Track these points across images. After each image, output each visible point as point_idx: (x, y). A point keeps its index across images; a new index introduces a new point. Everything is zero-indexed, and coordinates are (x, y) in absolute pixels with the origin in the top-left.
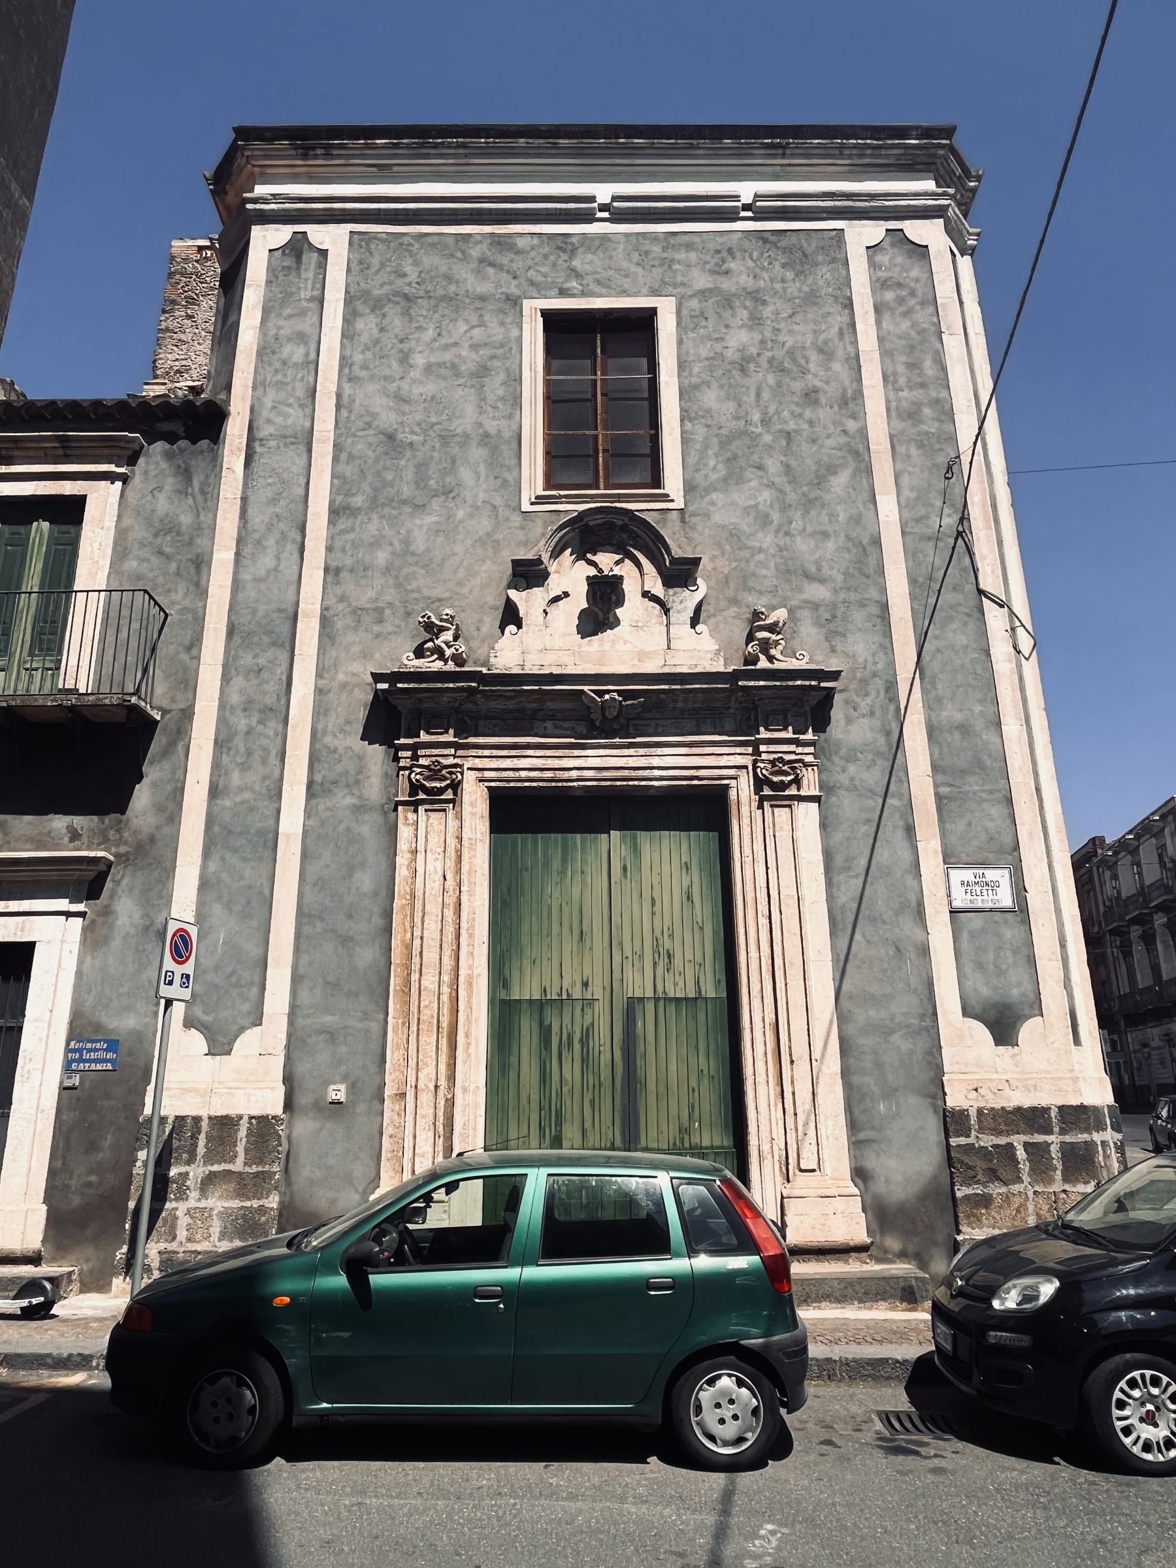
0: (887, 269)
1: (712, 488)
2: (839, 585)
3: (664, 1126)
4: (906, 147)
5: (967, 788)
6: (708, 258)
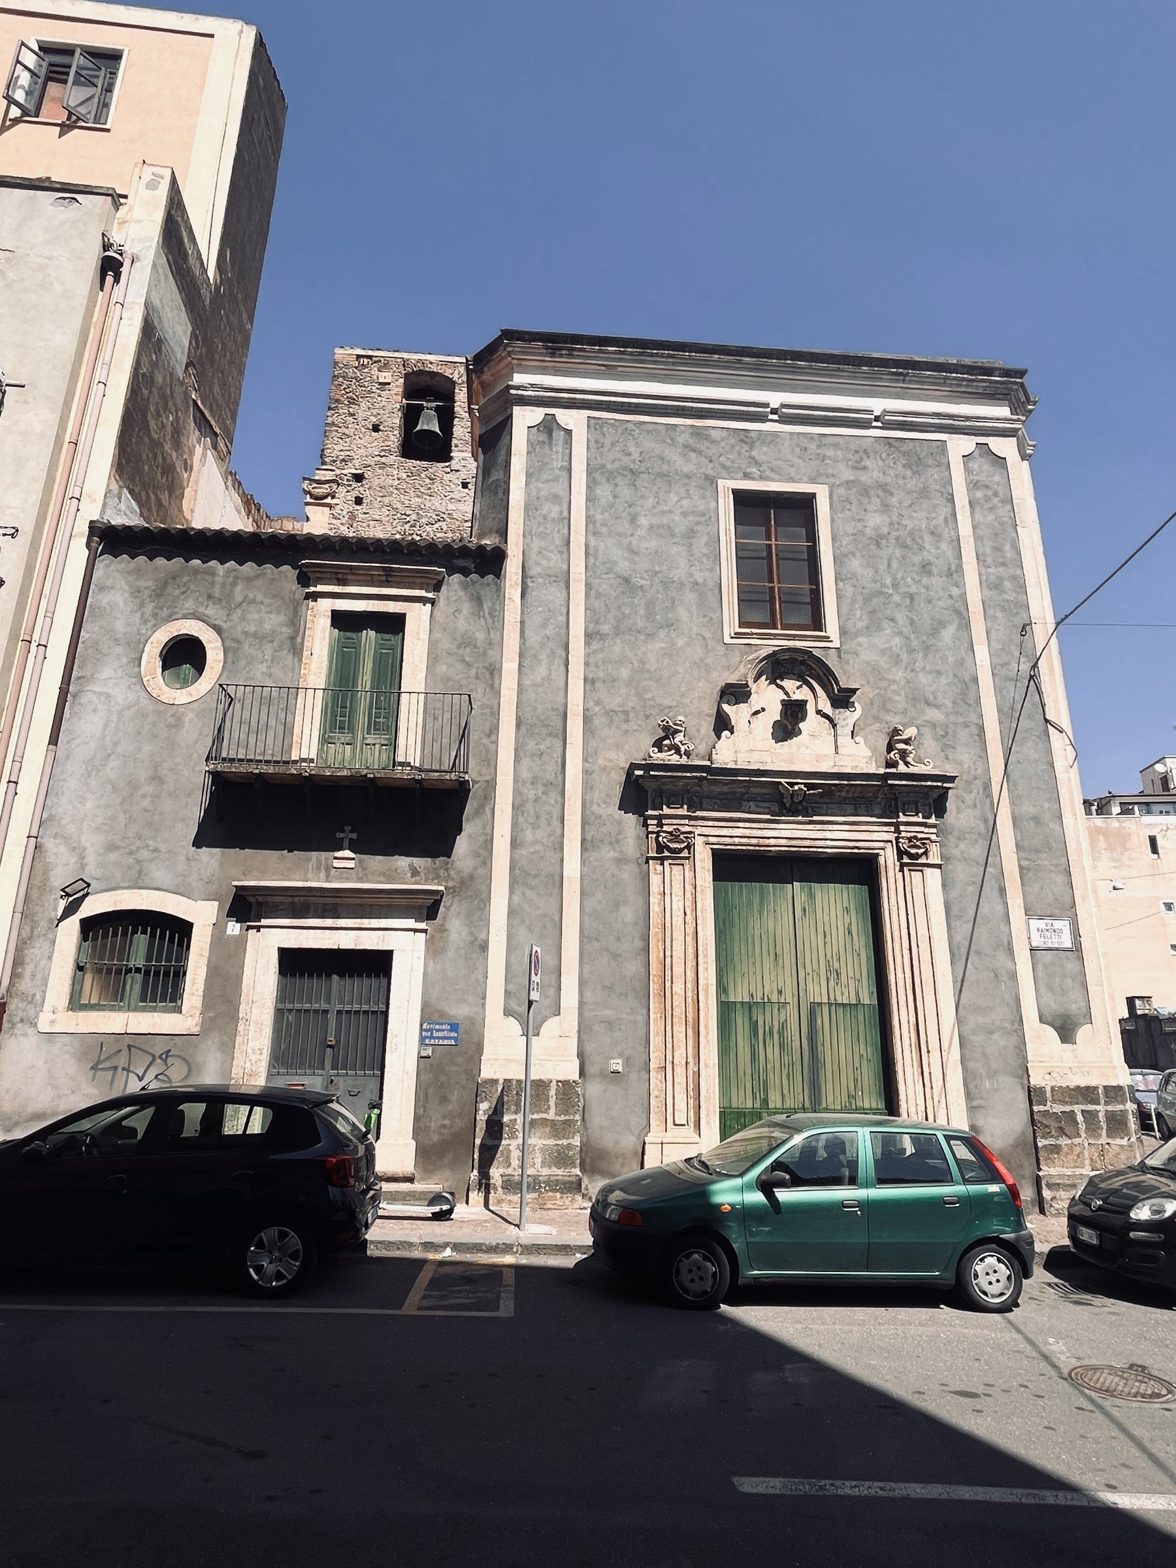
3: (837, 1093)
4: (990, 382)
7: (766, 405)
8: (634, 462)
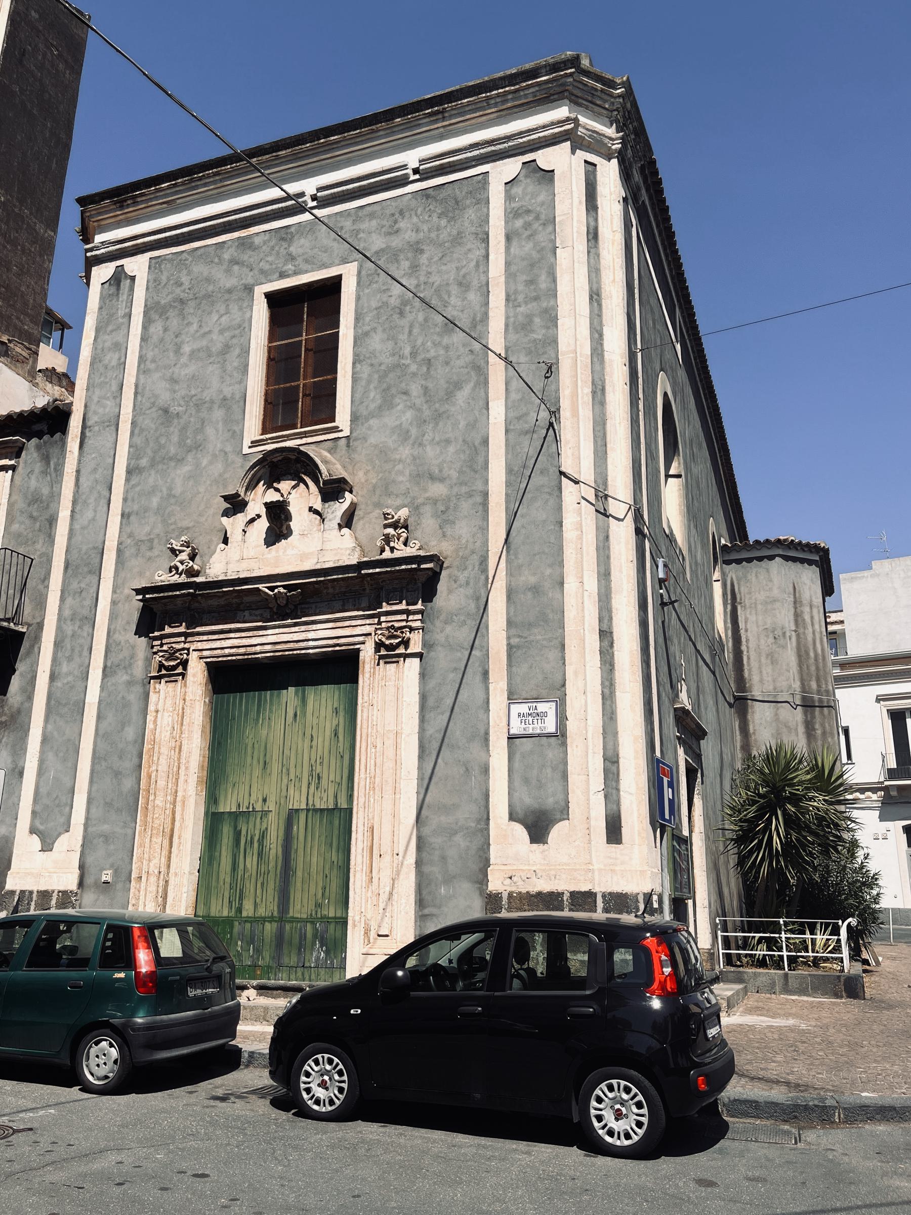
0: (520, 200)
1: (372, 415)
2: (455, 481)
3: (305, 901)
4: (538, 84)
5: (532, 638)
6: (385, 222)
7: (404, 167)
8: (184, 291)
